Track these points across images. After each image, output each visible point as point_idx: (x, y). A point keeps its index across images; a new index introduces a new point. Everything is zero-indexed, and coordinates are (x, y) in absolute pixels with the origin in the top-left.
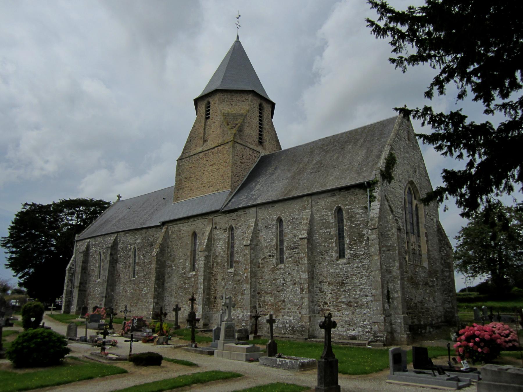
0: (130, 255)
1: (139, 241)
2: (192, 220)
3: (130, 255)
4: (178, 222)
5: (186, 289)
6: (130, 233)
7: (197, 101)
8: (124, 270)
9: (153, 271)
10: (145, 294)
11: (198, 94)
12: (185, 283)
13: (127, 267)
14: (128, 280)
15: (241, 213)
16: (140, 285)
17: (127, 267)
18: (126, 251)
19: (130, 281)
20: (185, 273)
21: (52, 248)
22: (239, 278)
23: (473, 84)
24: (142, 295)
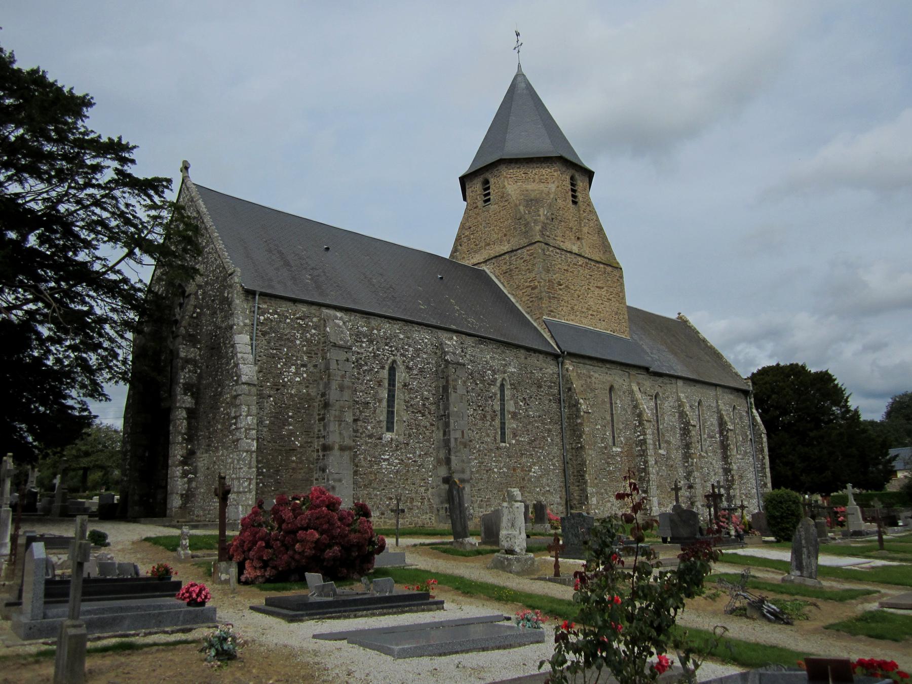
0: (495, 394)
1: (512, 369)
2: (608, 366)
3: (495, 394)
4: (587, 362)
5: (610, 473)
6: (490, 346)
7: (464, 181)
8: (480, 423)
9: (383, 595)
10: (538, 478)
11: (464, 168)
12: (608, 463)
13: (488, 418)
14: (493, 446)
15: (666, 380)
16: (524, 460)
17: (488, 418)
18: (483, 382)
19: (498, 448)
20: (606, 448)
21: (139, 294)
22: (672, 463)
23: (691, 665)
24: (529, 480)
